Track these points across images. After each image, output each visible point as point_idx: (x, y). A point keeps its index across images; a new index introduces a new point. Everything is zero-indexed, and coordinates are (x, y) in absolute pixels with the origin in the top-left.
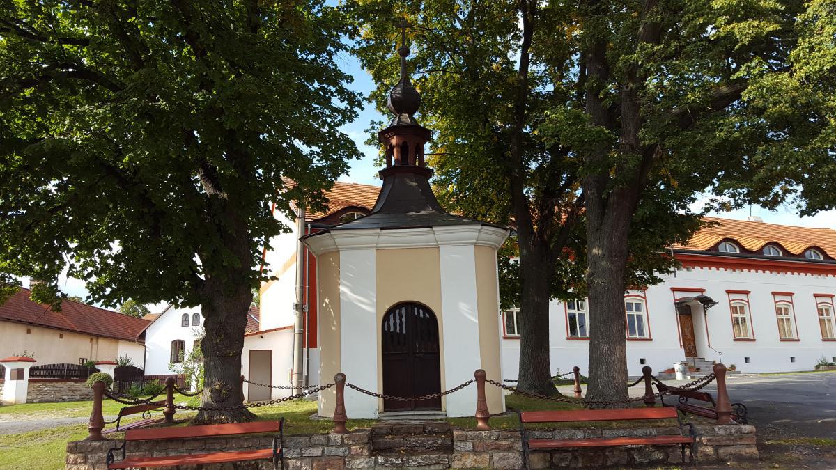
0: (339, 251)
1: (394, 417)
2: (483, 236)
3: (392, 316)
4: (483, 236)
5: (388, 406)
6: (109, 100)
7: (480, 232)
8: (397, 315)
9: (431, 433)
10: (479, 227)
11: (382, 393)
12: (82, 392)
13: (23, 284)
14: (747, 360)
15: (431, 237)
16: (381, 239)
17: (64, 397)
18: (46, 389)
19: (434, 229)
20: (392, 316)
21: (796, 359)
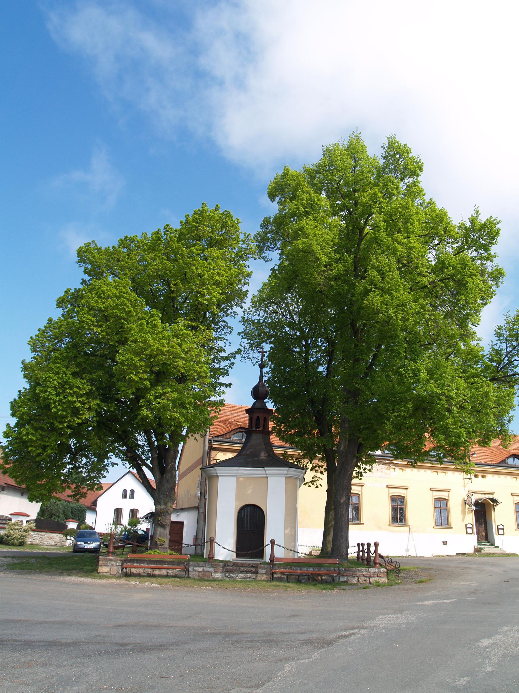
0: (218, 476)
1: (240, 561)
2: (290, 473)
3: (243, 511)
4: (290, 473)
5: (238, 556)
6: (88, 344)
7: (288, 471)
8: (246, 511)
9: (252, 566)
10: (287, 469)
11: (235, 550)
12: (55, 540)
13: (131, 235)
14: (445, 543)
15: (264, 472)
16: (286, 472)
17: (45, 542)
18: (34, 535)
19: (215, 468)
20: (243, 511)
21: (445, 540)
